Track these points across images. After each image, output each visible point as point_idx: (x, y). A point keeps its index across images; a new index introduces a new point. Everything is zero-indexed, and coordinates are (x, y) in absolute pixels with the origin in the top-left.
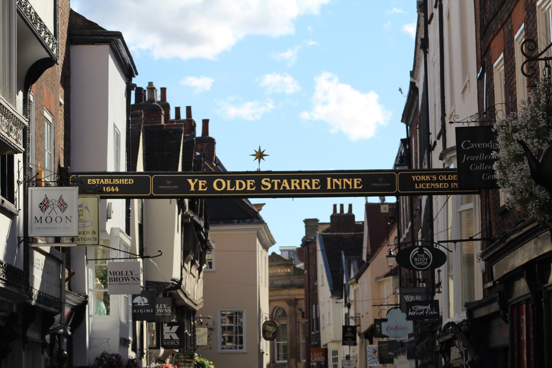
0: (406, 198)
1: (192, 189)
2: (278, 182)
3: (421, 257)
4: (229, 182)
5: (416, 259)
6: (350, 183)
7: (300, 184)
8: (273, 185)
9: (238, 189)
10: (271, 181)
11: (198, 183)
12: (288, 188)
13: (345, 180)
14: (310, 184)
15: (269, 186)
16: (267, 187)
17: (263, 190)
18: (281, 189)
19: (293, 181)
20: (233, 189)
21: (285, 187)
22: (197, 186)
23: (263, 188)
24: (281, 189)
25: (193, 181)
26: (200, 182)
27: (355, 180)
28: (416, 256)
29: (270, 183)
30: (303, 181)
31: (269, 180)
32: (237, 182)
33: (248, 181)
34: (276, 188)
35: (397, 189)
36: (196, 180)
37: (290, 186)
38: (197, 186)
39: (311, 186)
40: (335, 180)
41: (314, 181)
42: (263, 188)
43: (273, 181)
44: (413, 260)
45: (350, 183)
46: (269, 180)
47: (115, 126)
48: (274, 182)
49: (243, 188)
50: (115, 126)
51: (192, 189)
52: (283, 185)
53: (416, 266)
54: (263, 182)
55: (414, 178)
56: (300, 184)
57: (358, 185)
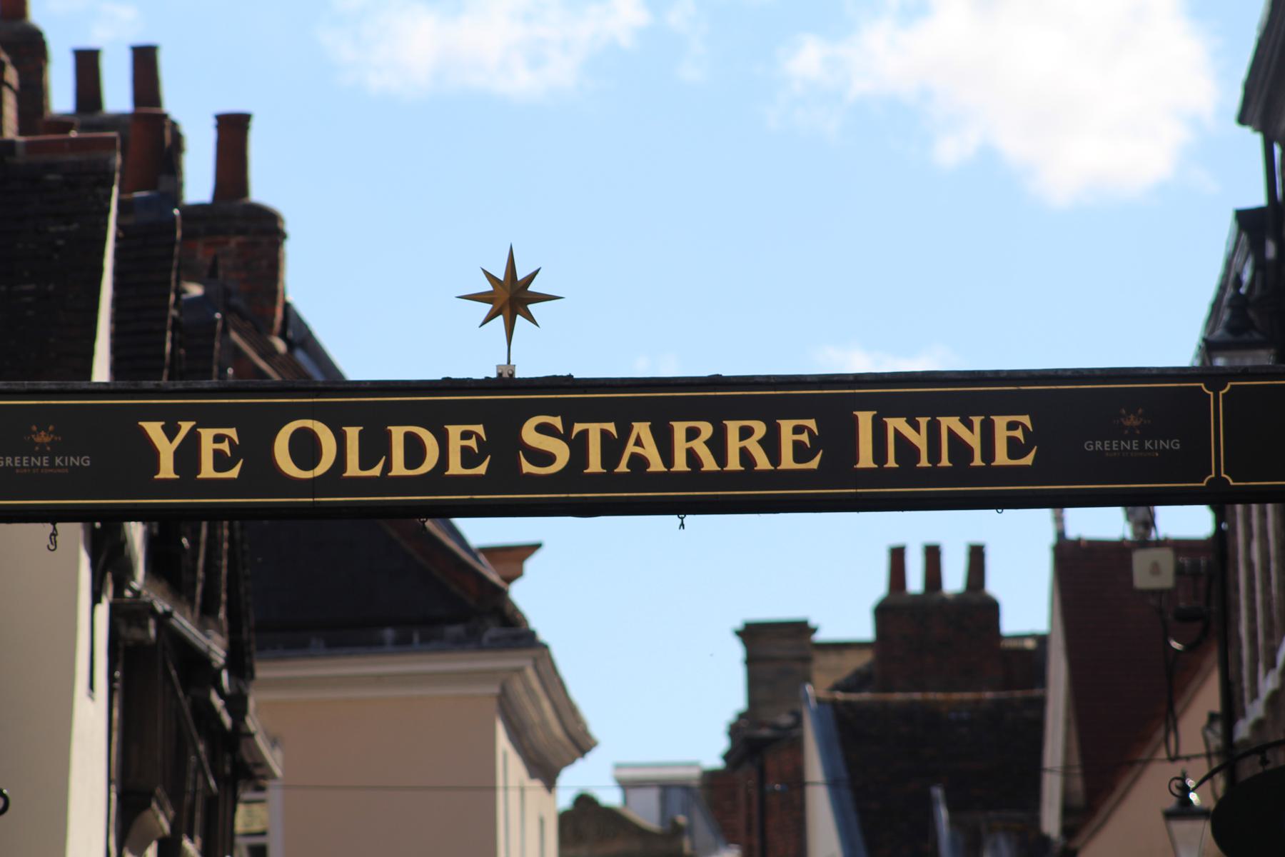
0: (1263, 514)
1: (167, 470)
2: (604, 434)
4: (353, 433)
6: (973, 439)
7: (718, 445)
8: (579, 447)
10: (568, 426)
12: (656, 465)
13: (950, 423)
14: (771, 444)
15: (562, 452)
16: (548, 458)
18: (623, 467)
19: (680, 428)
20: (376, 471)
21: (639, 462)
23: (527, 467)
24: (623, 467)
25: (171, 433)
26: (207, 435)
27: (1000, 422)
29: (565, 437)
31: (557, 422)
32: (398, 434)
33: (454, 431)
37: (667, 456)
39: (774, 456)
40: (896, 424)
41: (786, 426)
42: (527, 467)
43: (578, 427)
45: (973, 439)
46: (557, 422)
48: (585, 434)
51: (167, 470)
52: (631, 448)
54: (529, 434)
55: (166, 450)
56: (718, 445)
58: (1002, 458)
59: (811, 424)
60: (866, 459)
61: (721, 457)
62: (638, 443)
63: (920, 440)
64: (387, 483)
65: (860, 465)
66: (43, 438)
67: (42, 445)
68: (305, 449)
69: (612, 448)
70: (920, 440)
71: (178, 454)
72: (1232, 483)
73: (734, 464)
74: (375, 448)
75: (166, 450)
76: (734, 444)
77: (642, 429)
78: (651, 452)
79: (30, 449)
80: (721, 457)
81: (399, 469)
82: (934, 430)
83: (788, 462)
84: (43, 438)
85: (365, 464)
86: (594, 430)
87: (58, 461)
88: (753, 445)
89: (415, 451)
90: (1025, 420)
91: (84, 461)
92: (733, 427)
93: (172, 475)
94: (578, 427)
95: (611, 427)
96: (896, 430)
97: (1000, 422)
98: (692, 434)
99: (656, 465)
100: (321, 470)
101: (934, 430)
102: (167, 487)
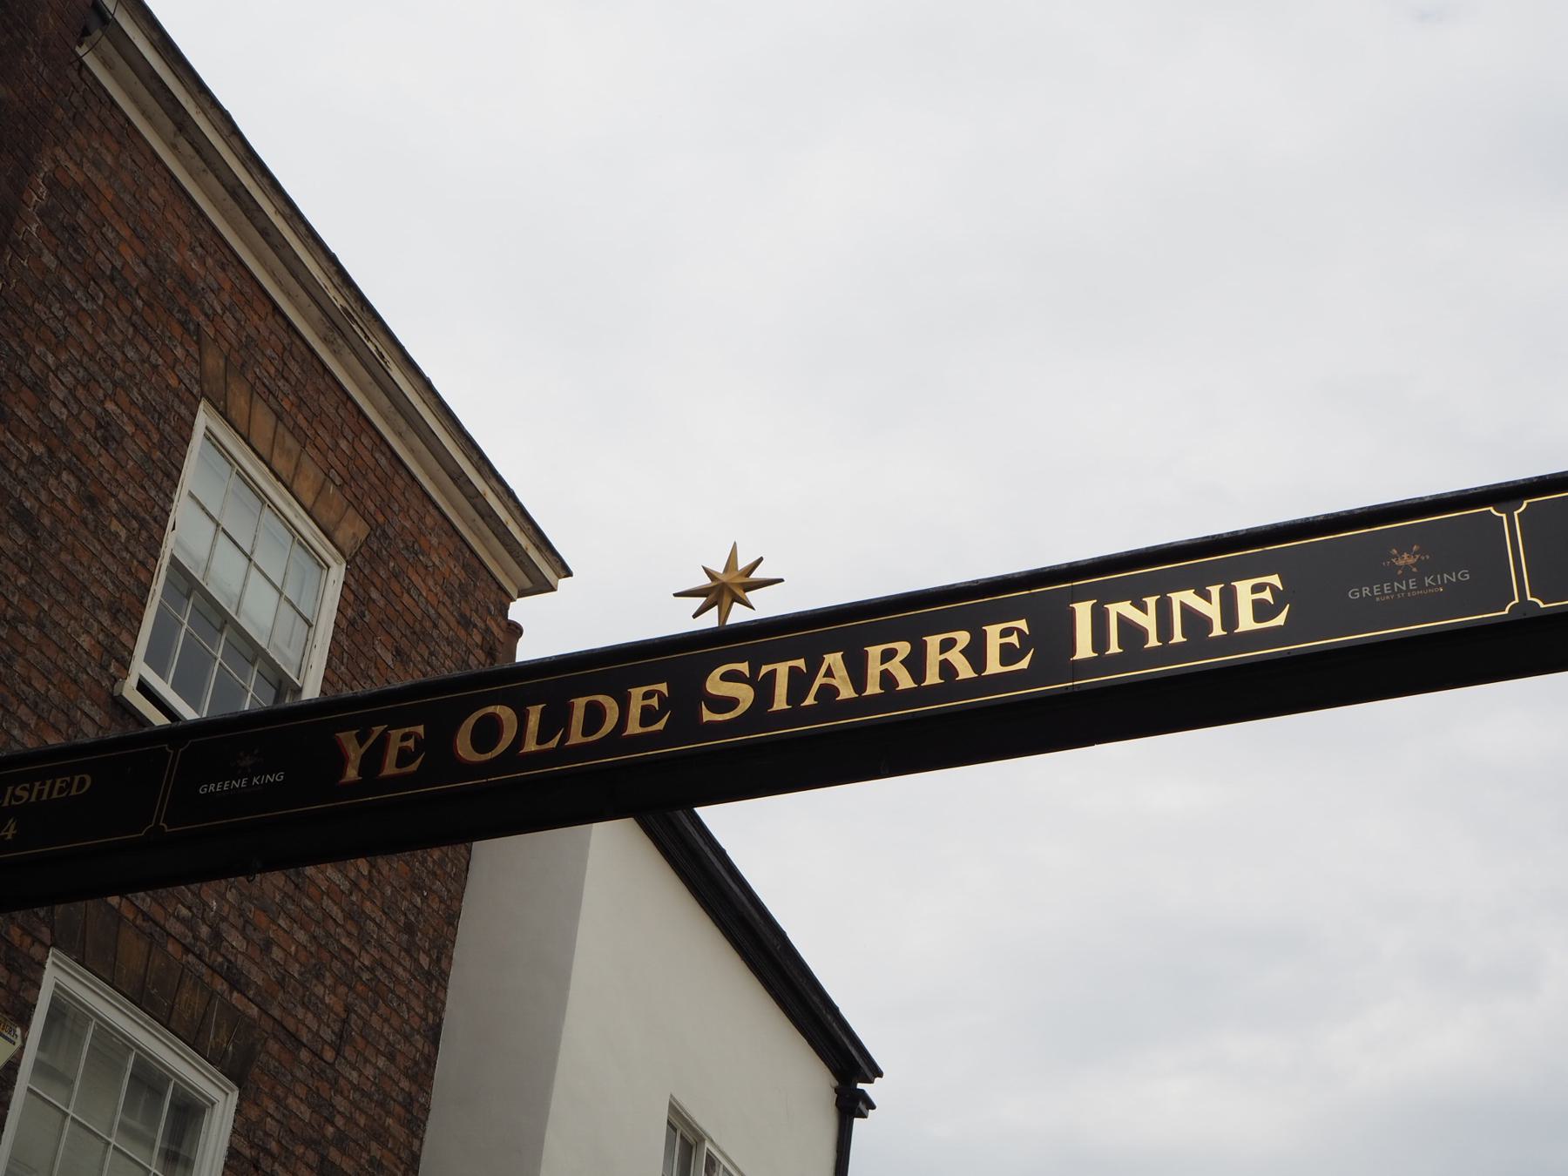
2: (793, 671)
4: (534, 714)
7: (915, 663)
8: (764, 688)
10: (754, 669)
11: (383, 740)
12: (846, 692)
14: (976, 653)
15: (745, 695)
20: (553, 743)
21: (828, 692)
23: (708, 716)
25: (361, 739)
27: (1243, 588)
31: (744, 667)
36: (378, 730)
37: (859, 680)
40: (1122, 608)
42: (708, 716)
43: (765, 669)
46: (744, 667)
48: (772, 675)
52: (820, 680)
56: (915, 663)
57: (1262, 611)
58: (1246, 622)
59: (1275, 579)
60: (1084, 649)
63: (1147, 621)
64: (565, 753)
65: (776, 707)
66: (1406, 560)
67: (1407, 568)
68: (487, 733)
69: (799, 683)
70: (1147, 621)
71: (365, 758)
72: (1542, 605)
73: (933, 677)
74: (555, 721)
76: (874, 668)
77: (834, 660)
79: (1391, 574)
81: (576, 737)
83: (994, 666)
84: (1406, 560)
87: (1428, 581)
89: (595, 716)
90: (1022, 624)
91: (279, 777)
92: (933, 642)
93: (878, 690)
94: (765, 669)
95: (800, 663)
96: (1182, 603)
97: (1243, 588)
99: (846, 692)
100: (501, 748)
102: (1087, 667)
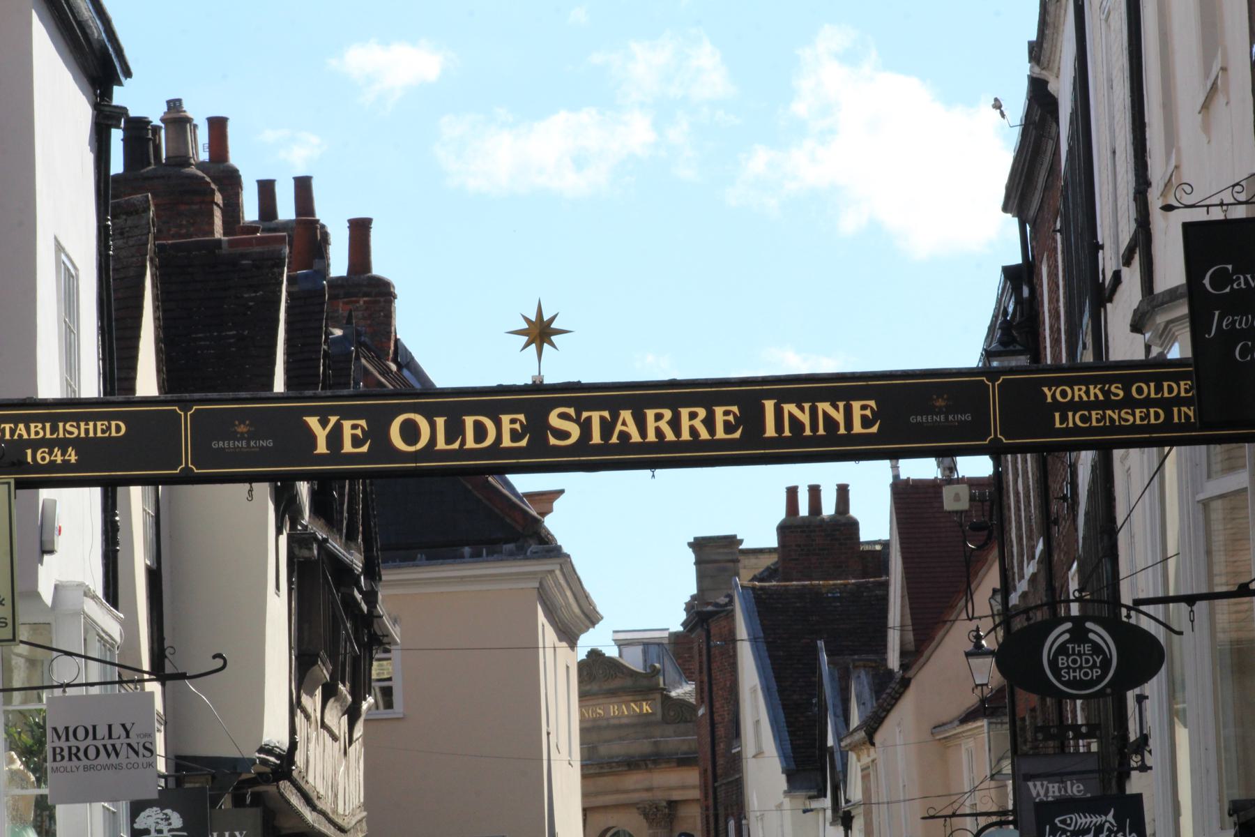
1: (322, 448)
2: (602, 419)
3: (1080, 655)
4: (440, 422)
5: (1062, 660)
6: (839, 417)
7: (675, 424)
8: (586, 426)
9: (470, 444)
10: (579, 414)
11: (338, 429)
12: (636, 438)
13: (824, 406)
14: (709, 422)
15: (575, 431)
17: (554, 446)
18: (614, 440)
19: (650, 414)
20: (456, 446)
21: (624, 436)
22: (335, 438)
23: (553, 441)
24: (614, 440)
25: (324, 423)
26: (347, 425)
27: (856, 405)
28: (1062, 650)
29: (577, 421)
30: (685, 412)
31: (571, 411)
34: (596, 438)
35: (995, 432)
38: (335, 438)
39: (712, 430)
40: (789, 408)
41: (719, 411)
42: (553, 441)
43: (585, 415)
44: (1053, 663)
45: (839, 417)
46: (571, 411)
47: (59, 248)
48: (589, 419)
49: (488, 442)
50: (59, 248)
52: (619, 427)
53: (1068, 684)
54: (554, 420)
55: (321, 434)
56: (675, 424)
61: (677, 432)
62: (624, 423)
69: (607, 427)
75: (321, 434)
76: (651, 425)
78: (632, 429)
80: (677, 432)
82: (814, 412)
85: (449, 441)
86: (596, 416)
88: (697, 423)
92: (685, 412)
94: (585, 415)
95: (606, 414)
98: (693, 416)
101: (814, 412)
